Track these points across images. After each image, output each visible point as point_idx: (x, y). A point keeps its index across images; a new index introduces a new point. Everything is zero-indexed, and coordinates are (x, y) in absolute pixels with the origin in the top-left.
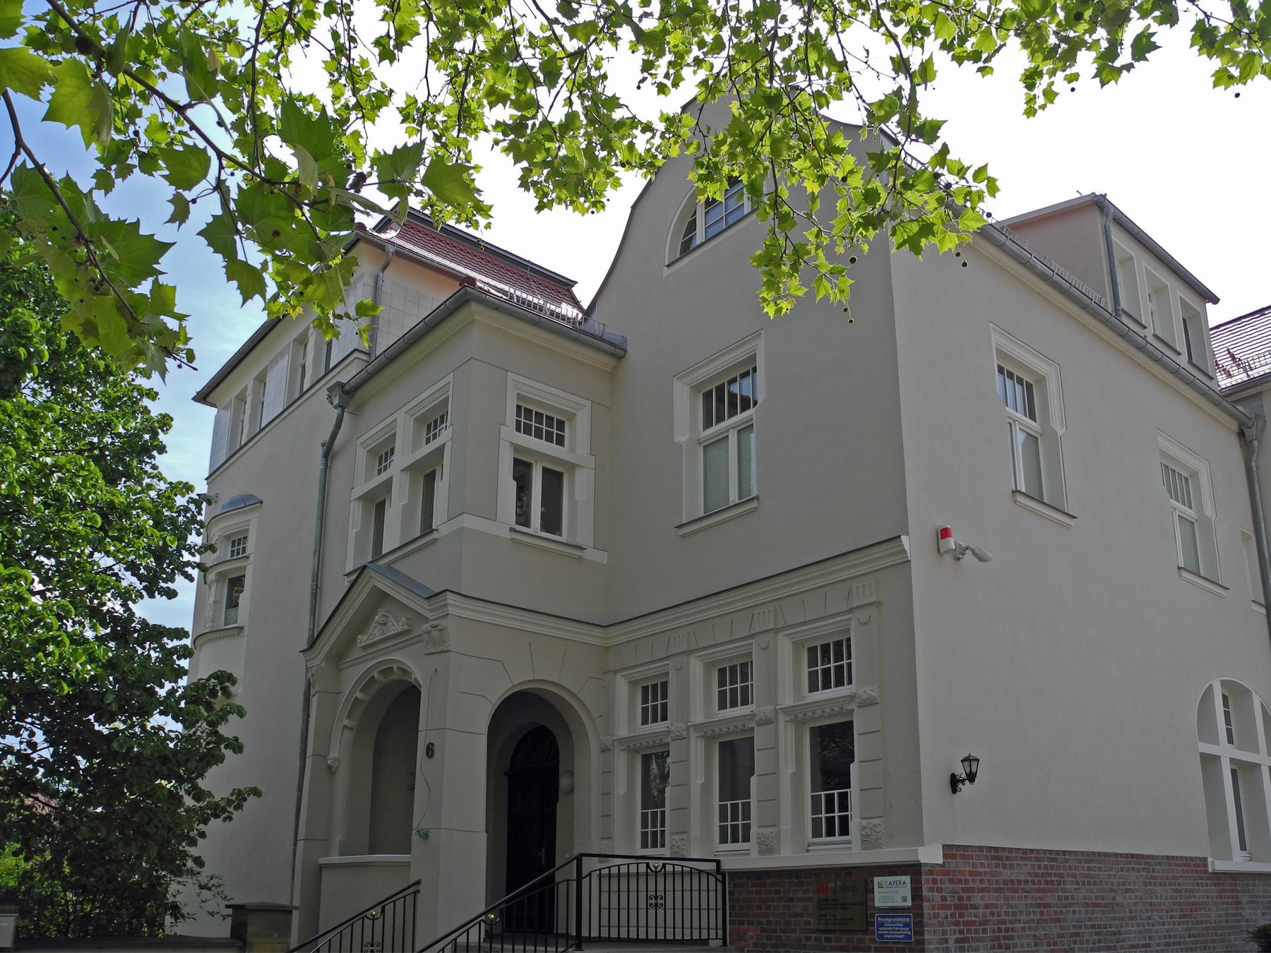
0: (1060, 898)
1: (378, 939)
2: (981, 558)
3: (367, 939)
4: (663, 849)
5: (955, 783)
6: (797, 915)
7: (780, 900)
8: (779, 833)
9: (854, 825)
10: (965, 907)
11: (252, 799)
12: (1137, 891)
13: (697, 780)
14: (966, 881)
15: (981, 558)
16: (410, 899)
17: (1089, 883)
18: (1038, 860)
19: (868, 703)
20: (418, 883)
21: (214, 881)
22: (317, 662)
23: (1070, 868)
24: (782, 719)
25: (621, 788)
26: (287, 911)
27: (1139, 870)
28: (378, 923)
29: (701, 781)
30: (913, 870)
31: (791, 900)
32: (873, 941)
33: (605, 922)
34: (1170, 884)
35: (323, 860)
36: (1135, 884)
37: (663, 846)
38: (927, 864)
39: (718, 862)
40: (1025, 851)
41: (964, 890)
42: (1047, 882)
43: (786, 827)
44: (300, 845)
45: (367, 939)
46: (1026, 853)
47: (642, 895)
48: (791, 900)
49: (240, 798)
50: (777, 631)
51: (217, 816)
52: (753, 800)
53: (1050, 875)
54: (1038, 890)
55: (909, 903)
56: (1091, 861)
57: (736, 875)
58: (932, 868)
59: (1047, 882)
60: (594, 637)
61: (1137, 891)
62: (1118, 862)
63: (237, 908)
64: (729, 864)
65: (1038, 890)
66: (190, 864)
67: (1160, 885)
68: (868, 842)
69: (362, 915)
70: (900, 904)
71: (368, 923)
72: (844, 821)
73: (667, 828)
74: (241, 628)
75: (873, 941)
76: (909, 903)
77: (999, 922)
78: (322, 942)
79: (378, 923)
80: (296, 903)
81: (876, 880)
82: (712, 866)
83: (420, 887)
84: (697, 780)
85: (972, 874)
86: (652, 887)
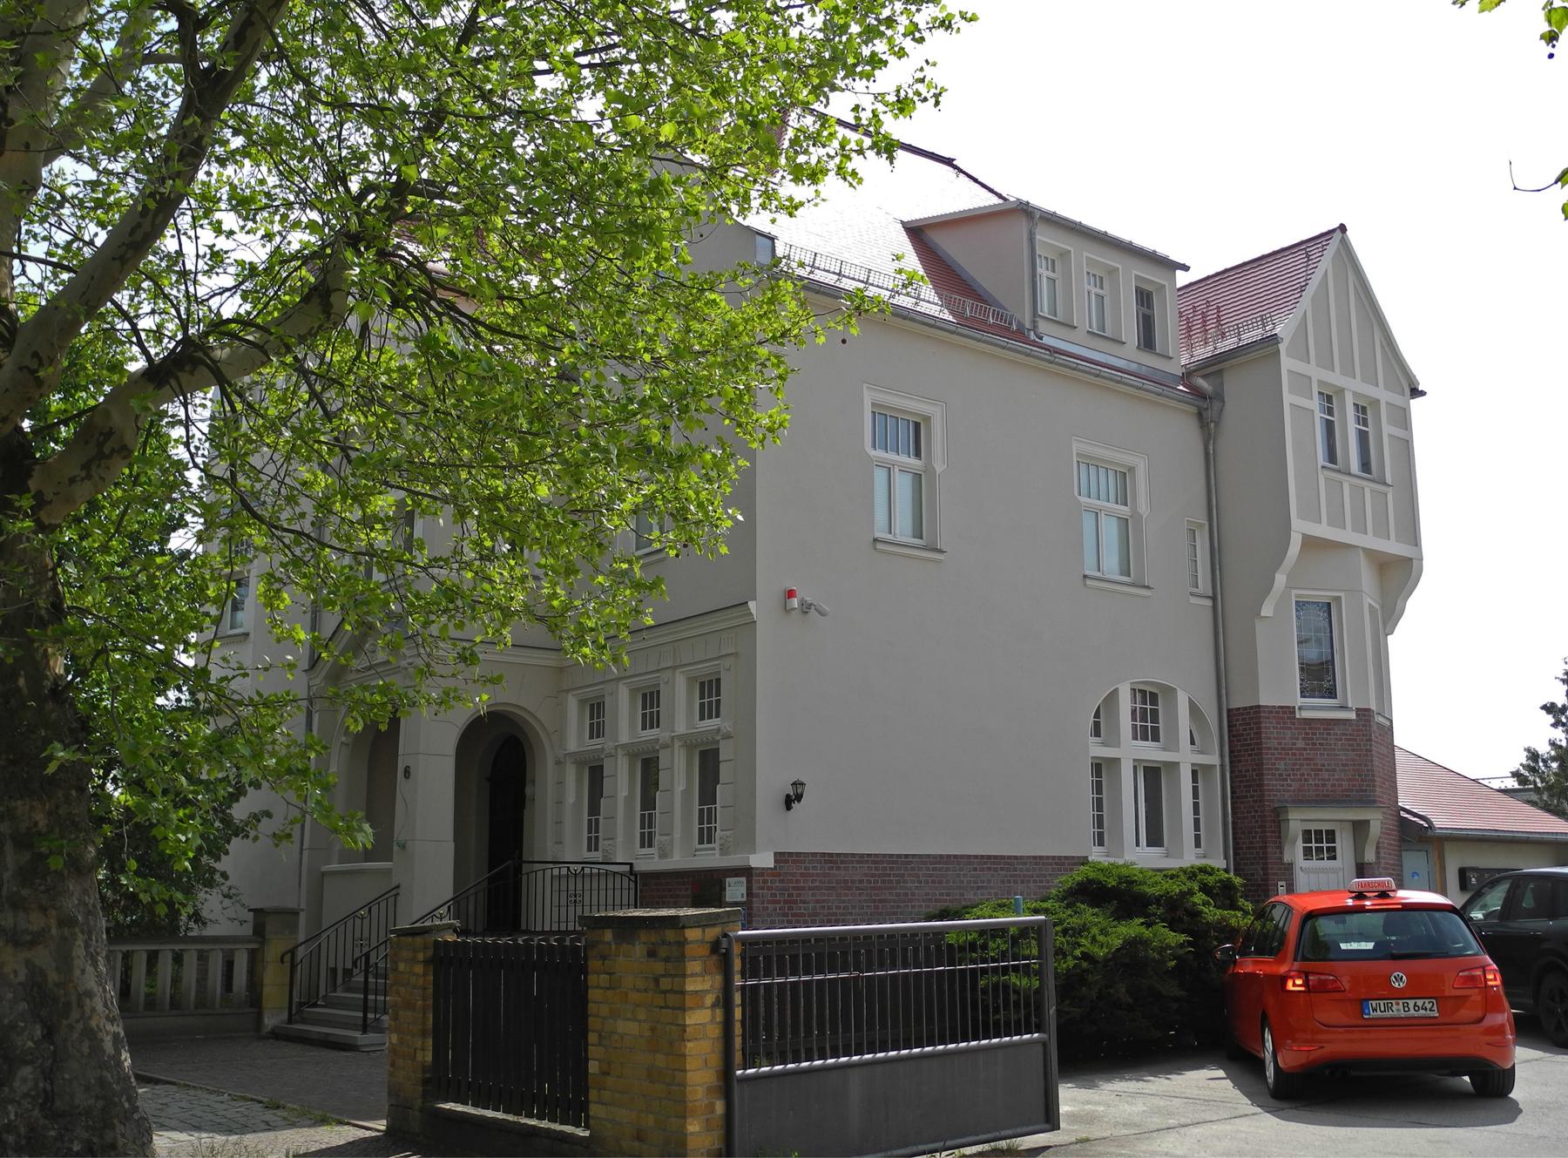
0: (898, 895)
1: (366, 934)
2: (822, 614)
3: (358, 935)
4: (1332, 862)
8: (672, 841)
10: (795, 902)
11: (265, 820)
12: (992, 888)
13: (623, 793)
14: (797, 881)
15: (822, 614)
16: (391, 900)
17: (933, 882)
18: (875, 862)
19: (728, 737)
20: (398, 887)
21: (233, 891)
22: (317, 681)
23: (913, 869)
24: (677, 744)
25: (570, 799)
26: (295, 913)
27: (996, 870)
28: (366, 922)
29: (625, 793)
30: (746, 872)
31: (678, 896)
33: (555, 918)
34: (1035, 881)
35: (325, 868)
36: (989, 881)
37: (597, 849)
38: (757, 869)
39: (631, 865)
40: (862, 856)
41: (794, 888)
42: (883, 882)
43: (677, 835)
44: (306, 853)
45: (358, 935)
46: (861, 858)
47: (563, 895)
49: (256, 818)
51: (237, 835)
53: (889, 875)
54: (874, 888)
56: (986, 863)
58: (763, 872)
59: (883, 882)
61: (992, 888)
62: (969, 863)
63: (257, 912)
64: (641, 866)
65: (874, 888)
66: (217, 876)
67: (1022, 882)
68: (724, 851)
69: (353, 915)
71: (358, 922)
73: (600, 834)
74: (247, 635)
77: (829, 914)
78: (324, 935)
79: (366, 922)
80: (303, 906)
82: (627, 868)
83: (400, 891)
84: (680, 787)
85: (802, 875)
86: (571, 887)
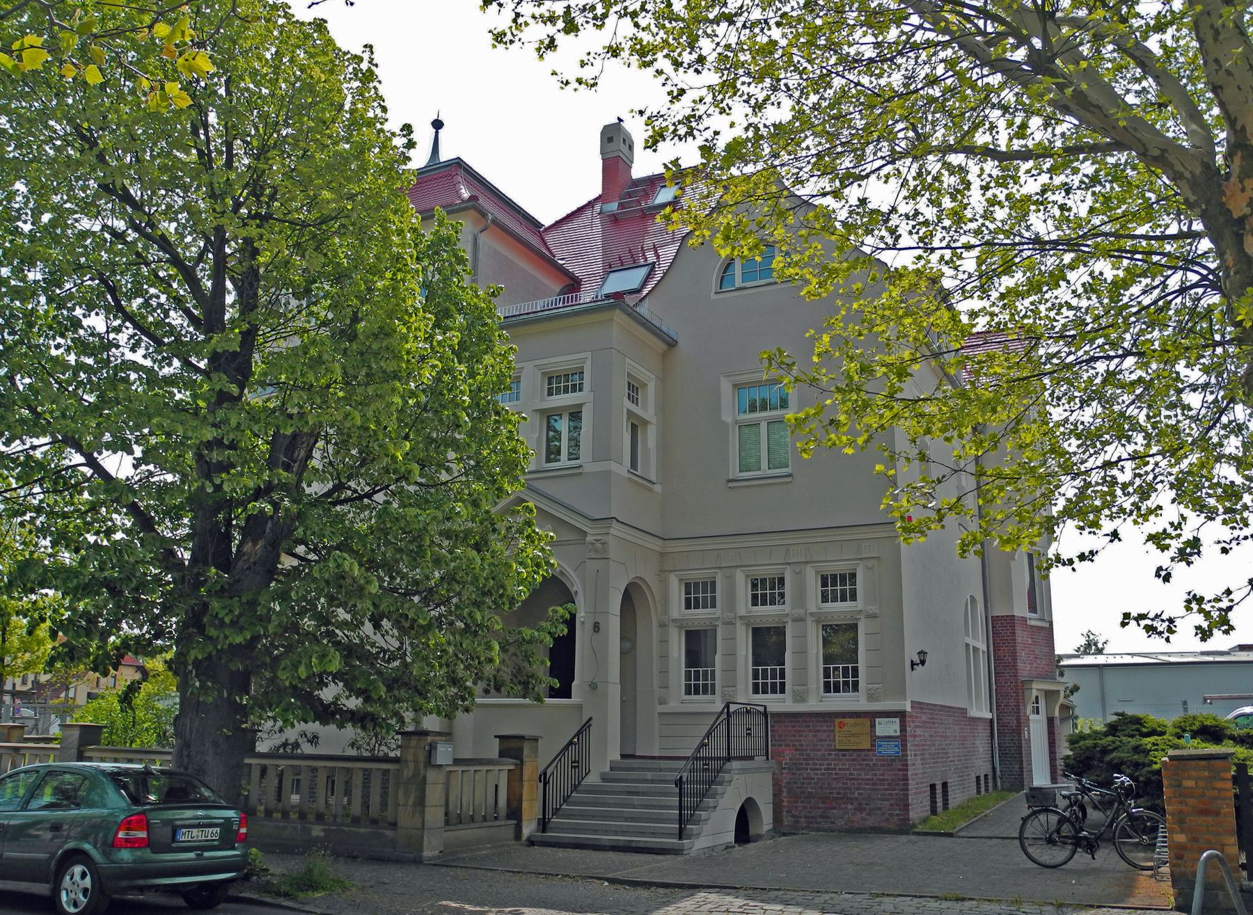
5: (913, 664)
6: (821, 741)
7: (810, 731)
9: (862, 685)
30: (901, 715)
32: (875, 755)
48: (819, 731)
50: (807, 563)
52: (861, 666)
55: (898, 734)
57: (775, 715)
60: (656, 545)
70: (893, 734)
72: (783, 685)
75: (875, 755)
76: (898, 734)
81: (877, 720)
